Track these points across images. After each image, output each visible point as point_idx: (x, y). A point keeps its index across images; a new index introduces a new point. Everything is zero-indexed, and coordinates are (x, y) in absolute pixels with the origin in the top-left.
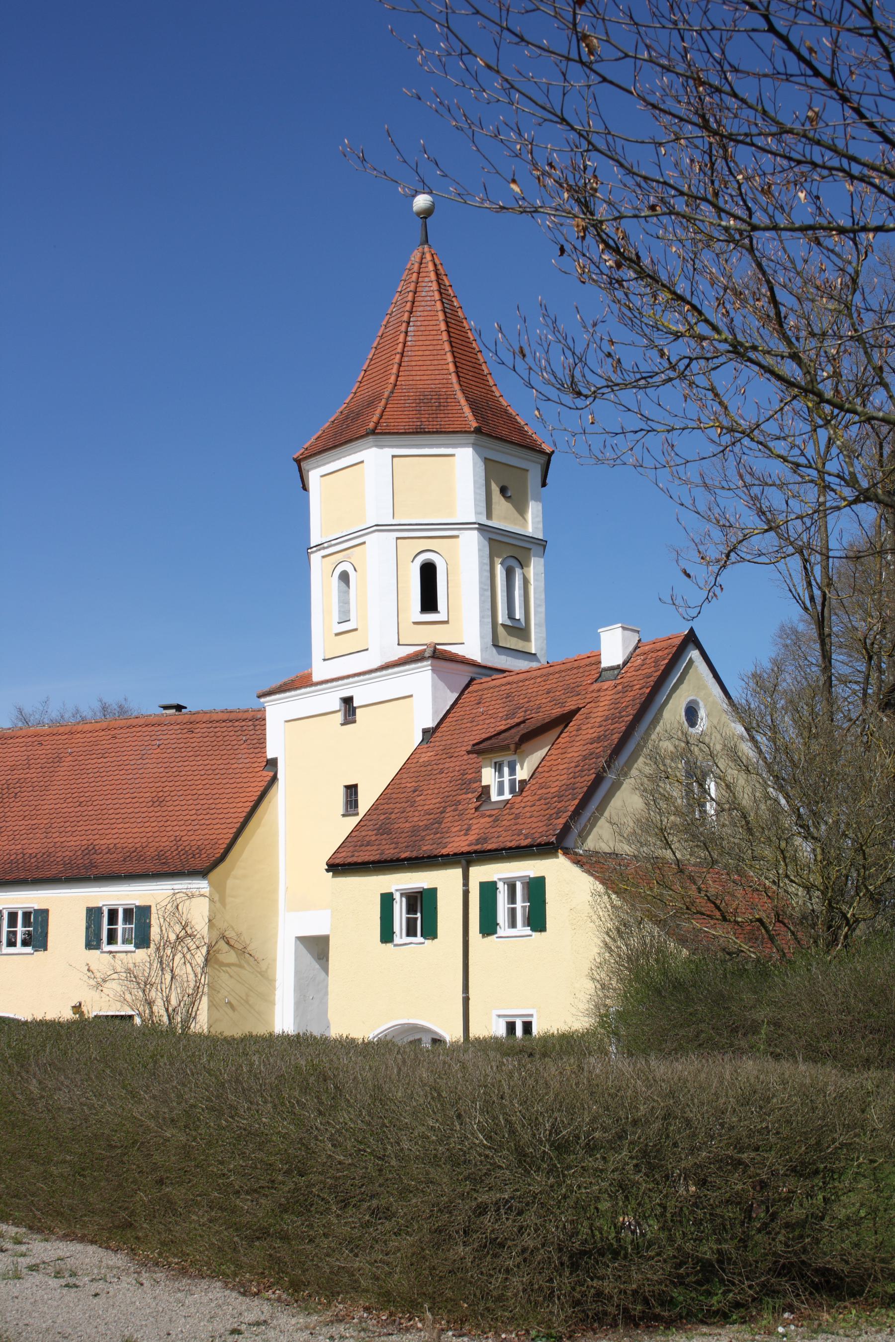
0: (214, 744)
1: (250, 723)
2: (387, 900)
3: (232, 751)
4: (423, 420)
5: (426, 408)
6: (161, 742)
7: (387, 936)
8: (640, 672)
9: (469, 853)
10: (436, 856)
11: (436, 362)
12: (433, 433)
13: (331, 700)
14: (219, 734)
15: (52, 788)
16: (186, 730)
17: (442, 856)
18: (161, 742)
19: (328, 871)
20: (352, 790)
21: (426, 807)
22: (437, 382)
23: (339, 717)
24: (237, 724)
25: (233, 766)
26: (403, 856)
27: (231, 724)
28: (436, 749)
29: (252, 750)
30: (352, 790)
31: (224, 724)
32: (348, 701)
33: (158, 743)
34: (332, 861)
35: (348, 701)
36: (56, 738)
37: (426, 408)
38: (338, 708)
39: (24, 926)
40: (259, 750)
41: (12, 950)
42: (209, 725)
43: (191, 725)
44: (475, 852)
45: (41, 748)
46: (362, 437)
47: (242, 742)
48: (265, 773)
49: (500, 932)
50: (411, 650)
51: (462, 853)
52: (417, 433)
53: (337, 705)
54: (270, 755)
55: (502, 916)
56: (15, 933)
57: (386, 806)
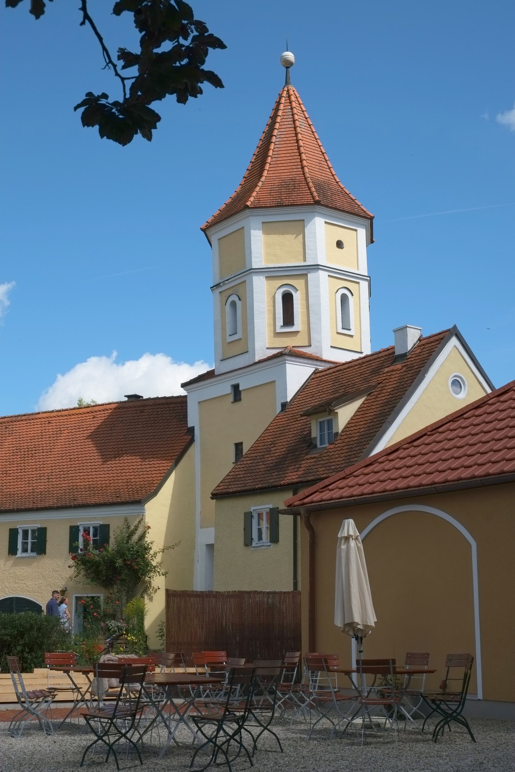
0: (156, 419)
1: (180, 405)
2: (248, 516)
3: (166, 424)
4: (283, 198)
5: (285, 190)
6: (123, 419)
7: (248, 542)
8: (419, 357)
9: (297, 483)
10: (277, 486)
11: (293, 161)
12: (288, 205)
13: (226, 388)
14: (159, 413)
15: (55, 450)
16: (139, 411)
17: (281, 486)
18: (123, 419)
19: (212, 498)
20: (239, 446)
21: (276, 454)
22: (294, 173)
23: (231, 398)
24: (171, 406)
25: (167, 433)
26: (257, 487)
27: (167, 406)
28: (288, 416)
29: (179, 422)
30: (239, 446)
31: (163, 406)
32: (236, 388)
33: (121, 419)
34: (215, 492)
35: (236, 388)
36: (60, 418)
37: (285, 190)
38: (230, 392)
39: (32, 539)
40: (183, 422)
41: (25, 555)
42: (154, 407)
43: (143, 408)
44: (301, 482)
45: (49, 425)
46: (241, 211)
47: (173, 417)
48: (186, 437)
49: (254, 544)
50: (275, 352)
51: (293, 483)
52: (278, 206)
53: (228, 390)
54: (190, 425)
55: (20, 546)
56: (27, 543)
57: (253, 455)
